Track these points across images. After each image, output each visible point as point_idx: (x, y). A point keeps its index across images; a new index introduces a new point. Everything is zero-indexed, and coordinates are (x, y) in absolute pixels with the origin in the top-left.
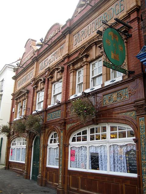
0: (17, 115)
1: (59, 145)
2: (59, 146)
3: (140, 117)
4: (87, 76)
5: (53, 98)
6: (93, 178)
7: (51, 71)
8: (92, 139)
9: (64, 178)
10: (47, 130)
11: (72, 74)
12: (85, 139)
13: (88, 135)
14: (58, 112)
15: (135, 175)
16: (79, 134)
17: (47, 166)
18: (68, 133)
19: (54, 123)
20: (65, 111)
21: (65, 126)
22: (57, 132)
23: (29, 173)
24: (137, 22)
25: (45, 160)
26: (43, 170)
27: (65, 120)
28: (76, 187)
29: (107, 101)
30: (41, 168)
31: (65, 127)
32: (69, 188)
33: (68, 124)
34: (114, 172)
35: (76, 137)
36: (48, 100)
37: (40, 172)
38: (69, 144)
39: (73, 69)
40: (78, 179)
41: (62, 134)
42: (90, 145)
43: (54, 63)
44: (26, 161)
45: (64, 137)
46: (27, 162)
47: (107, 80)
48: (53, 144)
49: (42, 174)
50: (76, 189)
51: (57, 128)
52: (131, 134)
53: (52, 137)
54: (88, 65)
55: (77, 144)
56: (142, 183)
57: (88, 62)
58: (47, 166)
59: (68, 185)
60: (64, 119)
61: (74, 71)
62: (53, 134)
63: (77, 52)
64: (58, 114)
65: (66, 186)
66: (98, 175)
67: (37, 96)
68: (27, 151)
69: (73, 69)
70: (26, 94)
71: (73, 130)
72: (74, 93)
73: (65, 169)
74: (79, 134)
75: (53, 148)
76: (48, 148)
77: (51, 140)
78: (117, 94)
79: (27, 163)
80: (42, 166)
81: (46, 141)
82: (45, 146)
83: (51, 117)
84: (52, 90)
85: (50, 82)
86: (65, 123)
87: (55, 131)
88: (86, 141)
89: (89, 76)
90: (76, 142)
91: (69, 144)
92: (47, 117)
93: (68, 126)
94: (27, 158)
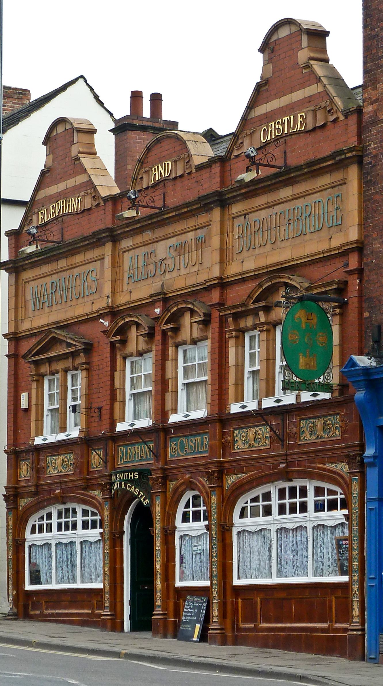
0: (42, 420)
1: (208, 527)
2: (102, 537)
3: (353, 477)
4: (267, 360)
5: (130, 400)
6: (283, 595)
7: (271, 282)
8: (282, 510)
9: (223, 606)
10: (171, 485)
11: (232, 342)
12: (50, 528)
13: (55, 521)
14: (202, 439)
15: (345, 579)
16: (255, 500)
17: (176, 586)
18: (229, 498)
19: (193, 467)
20: (220, 440)
21: (221, 479)
22: (199, 490)
23: (119, 615)
24: (358, 279)
25: (170, 572)
26: (166, 597)
27: (166, 470)
28: (251, 622)
29: (307, 434)
30: (162, 591)
31: (17, 504)
32: (237, 626)
33: (230, 472)
34: (251, 580)
35: (249, 508)
36: (169, 397)
37: (159, 603)
38: (232, 525)
39: (235, 330)
40: (256, 602)
41: (214, 499)
42: (279, 527)
43: (180, 284)
44: (107, 578)
45: (219, 507)
46: (110, 580)
47: (267, 396)
48: (191, 524)
49: (164, 606)
50: (326, 625)
51: (200, 482)
52: (345, 504)
53: (187, 506)
54: (41, 381)
55: (251, 523)
56: (352, 588)
57: (270, 323)
58: (176, 586)
59: (233, 622)
60: (13, 488)
61: (269, 327)
62: (188, 495)
63: (256, 277)
64: (202, 443)
65: (229, 621)
66: (189, 589)
67: (124, 371)
68: (107, 547)
69: (235, 330)
70: (82, 354)
71: (240, 489)
72: (240, 398)
73: (225, 584)
74: (255, 500)
75: (191, 534)
76: (177, 535)
77: (34, 527)
78: (324, 423)
79: (110, 585)
80: (163, 586)
81: (169, 517)
82: (169, 534)
83: (177, 450)
84: (177, 367)
85: (170, 342)
86: (221, 472)
87: (193, 490)
88: (307, 512)
89: (274, 360)
90: (326, 514)
91: (233, 524)
92: (169, 449)
93: (230, 481)
94: (110, 569)
